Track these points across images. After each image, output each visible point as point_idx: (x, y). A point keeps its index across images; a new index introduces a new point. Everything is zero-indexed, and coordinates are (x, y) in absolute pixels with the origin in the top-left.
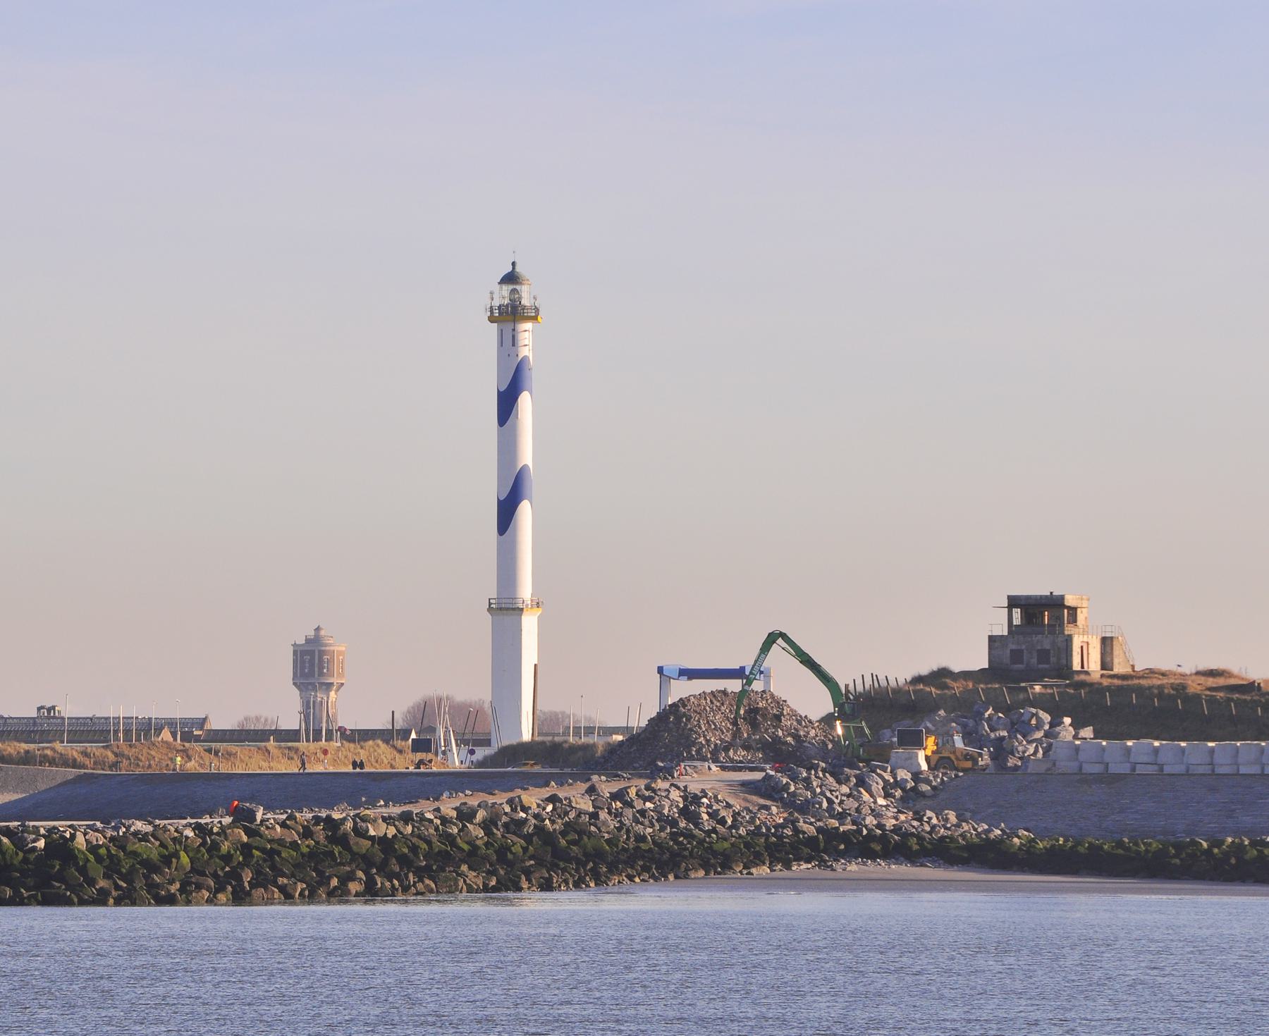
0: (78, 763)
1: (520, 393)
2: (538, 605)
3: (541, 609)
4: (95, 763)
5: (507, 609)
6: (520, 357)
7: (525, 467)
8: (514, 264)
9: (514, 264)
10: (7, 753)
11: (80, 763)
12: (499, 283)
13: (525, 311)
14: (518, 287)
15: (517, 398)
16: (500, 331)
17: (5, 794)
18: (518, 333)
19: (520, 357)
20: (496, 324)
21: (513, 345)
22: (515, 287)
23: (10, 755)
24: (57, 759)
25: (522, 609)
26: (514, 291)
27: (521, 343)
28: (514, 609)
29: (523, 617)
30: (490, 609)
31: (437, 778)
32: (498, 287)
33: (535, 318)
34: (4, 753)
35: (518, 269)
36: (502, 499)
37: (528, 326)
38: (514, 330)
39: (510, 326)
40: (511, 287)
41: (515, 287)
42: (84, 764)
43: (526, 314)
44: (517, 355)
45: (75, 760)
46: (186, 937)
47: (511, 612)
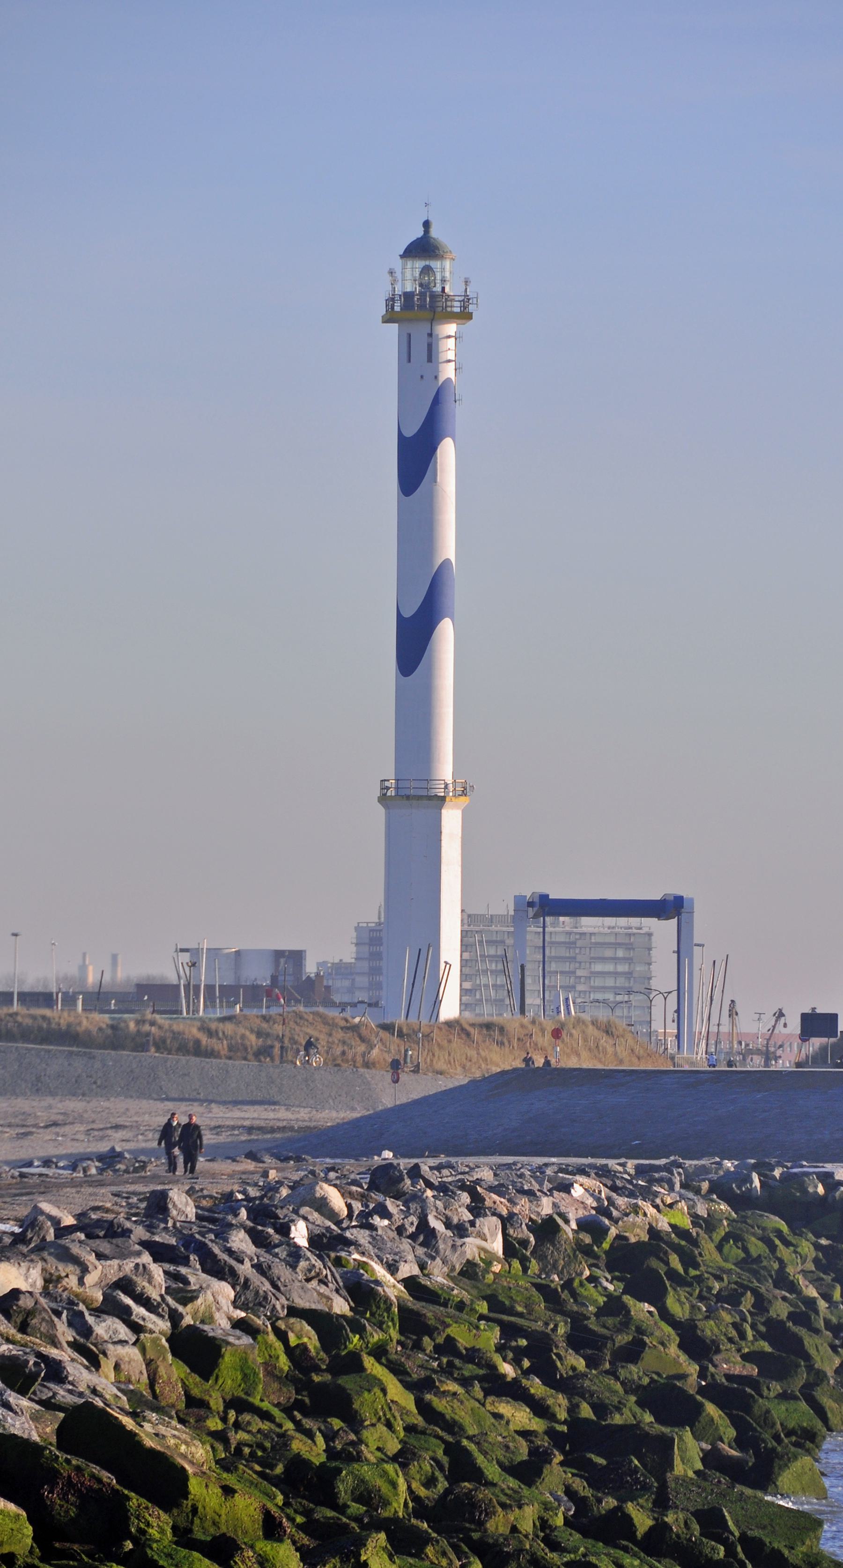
0: (203, 1048)
1: (441, 440)
2: (464, 793)
3: (467, 798)
4: (231, 1048)
5: (419, 798)
6: (441, 379)
7: (447, 562)
8: (427, 225)
9: (427, 225)
10: (83, 1028)
11: (207, 1046)
12: (402, 256)
13: (449, 303)
14: (435, 264)
15: (434, 449)
16: (405, 339)
17: (112, 1099)
18: (438, 339)
19: (441, 379)
20: (396, 325)
21: (430, 359)
22: (427, 263)
23: (88, 1032)
24: (168, 1041)
25: (443, 799)
26: (427, 270)
27: (443, 357)
28: (430, 798)
29: (444, 811)
30: (383, 799)
31: (676, 1075)
32: (400, 261)
33: (465, 316)
34: (78, 1028)
35: (434, 233)
36: (408, 613)
37: (451, 328)
38: (430, 335)
39: (419, 331)
40: (419, 264)
41: (427, 263)
42: (213, 1051)
43: (449, 309)
44: (436, 377)
45: (197, 1042)
46: (271, 1346)
47: (425, 802)
